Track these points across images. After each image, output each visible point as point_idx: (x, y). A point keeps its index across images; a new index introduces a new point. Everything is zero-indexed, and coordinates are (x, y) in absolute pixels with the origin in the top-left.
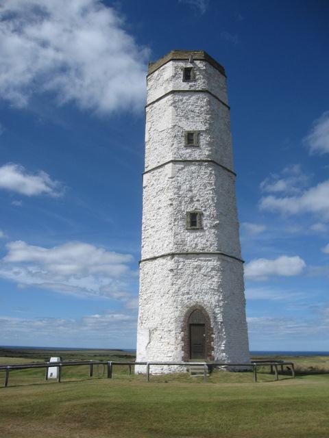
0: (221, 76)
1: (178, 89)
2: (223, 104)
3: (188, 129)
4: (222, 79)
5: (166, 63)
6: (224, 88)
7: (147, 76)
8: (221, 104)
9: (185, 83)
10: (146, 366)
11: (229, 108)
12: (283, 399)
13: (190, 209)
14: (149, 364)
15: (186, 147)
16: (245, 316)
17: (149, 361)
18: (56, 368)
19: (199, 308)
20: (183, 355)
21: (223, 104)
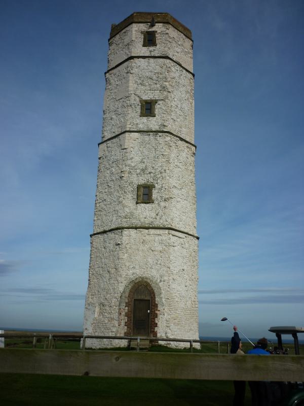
0: (187, 40)
1: (138, 55)
2: (187, 70)
3: (145, 98)
4: (188, 43)
5: (127, 26)
6: (189, 53)
7: (109, 40)
8: (184, 71)
9: (145, 49)
10: (189, 344)
11: (194, 75)
12: (180, 380)
13: (142, 180)
14: (85, 337)
15: (142, 115)
16: (154, 295)
17: (191, 339)
18: (127, 340)
19: (145, 284)
20: (126, 331)
21: (187, 70)
